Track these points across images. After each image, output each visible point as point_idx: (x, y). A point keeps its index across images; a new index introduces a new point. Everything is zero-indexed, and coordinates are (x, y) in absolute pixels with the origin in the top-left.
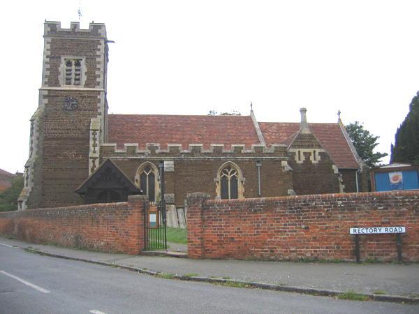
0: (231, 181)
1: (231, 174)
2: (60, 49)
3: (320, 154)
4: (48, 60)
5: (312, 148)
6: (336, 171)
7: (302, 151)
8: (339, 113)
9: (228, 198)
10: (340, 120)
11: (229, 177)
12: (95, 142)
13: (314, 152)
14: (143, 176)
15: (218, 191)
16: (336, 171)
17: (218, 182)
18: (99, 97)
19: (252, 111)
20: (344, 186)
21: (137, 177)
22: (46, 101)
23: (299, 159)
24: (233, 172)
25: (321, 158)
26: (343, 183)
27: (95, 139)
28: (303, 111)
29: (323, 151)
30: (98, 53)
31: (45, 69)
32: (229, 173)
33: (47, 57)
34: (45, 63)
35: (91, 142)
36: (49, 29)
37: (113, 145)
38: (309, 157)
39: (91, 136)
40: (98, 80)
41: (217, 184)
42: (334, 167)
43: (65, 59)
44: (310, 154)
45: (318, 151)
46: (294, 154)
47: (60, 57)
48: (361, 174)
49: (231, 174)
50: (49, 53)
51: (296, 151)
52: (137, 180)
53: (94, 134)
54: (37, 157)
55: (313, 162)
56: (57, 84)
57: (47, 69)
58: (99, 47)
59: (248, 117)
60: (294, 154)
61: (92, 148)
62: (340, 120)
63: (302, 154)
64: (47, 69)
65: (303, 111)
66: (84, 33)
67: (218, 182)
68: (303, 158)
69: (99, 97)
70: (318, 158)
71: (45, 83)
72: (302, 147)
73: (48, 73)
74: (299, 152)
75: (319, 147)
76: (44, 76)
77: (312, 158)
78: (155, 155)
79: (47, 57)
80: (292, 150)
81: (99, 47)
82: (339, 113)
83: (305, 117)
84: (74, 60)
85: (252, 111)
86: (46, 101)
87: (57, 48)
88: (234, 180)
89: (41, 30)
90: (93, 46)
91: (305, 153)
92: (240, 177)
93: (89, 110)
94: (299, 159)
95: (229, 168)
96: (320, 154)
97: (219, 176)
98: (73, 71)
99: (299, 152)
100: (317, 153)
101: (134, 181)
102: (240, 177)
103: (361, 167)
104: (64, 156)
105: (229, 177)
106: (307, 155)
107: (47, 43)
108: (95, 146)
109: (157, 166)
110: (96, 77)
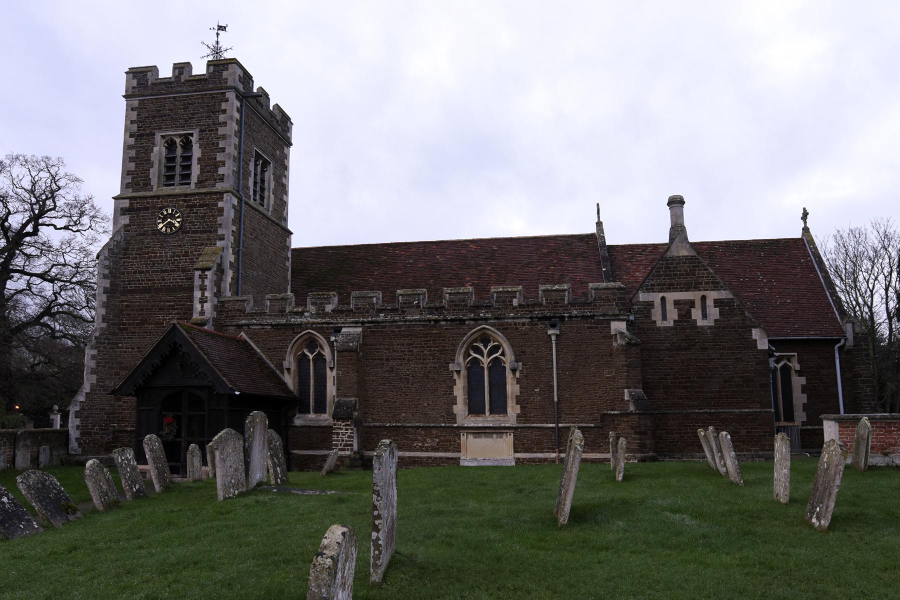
0: (490, 369)
1: (489, 355)
2: (154, 117)
3: (718, 303)
4: (132, 141)
5: (697, 288)
6: (763, 344)
7: (672, 296)
8: (805, 215)
9: (839, 413)
10: (806, 230)
11: (485, 361)
12: (203, 294)
13: (704, 298)
14: (302, 361)
15: (459, 390)
16: (763, 344)
17: (458, 372)
18: (220, 204)
19: (599, 224)
20: (802, 380)
21: (290, 361)
22: (125, 220)
23: (664, 318)
24: (495, 349)
25: (721, 313)
26: (800, 373)
27: (203, 288)
28: (676, 203)
29: (724, 294)
30: (222, 118)
31: (127, 159)
32: (485, 352)
33: (131, 136)
34: (127, 147)
35: (197, 294)
36: (135, 83)
37: (794, 354)
38: (689, 313)
39: (197, 282)
40: (221, 171)
41: (455, 376)
42: (756, 334)
43: (163, 137)
44: (692, 304)
45: (712, 295)
46: (651, 304)
47: (154, 134)
48: (849, 352)
49: (489, 355)
50: (135, 127)
51: (656, 297)
52: (289, 370)
53: (203, 278)
54: (104, 325)
55: (700, 323)
56: (147, 185)
57: (131, 159)
58: (224, 106)
59: (591, 236)
60: (651, 304)
61: (198, 306)
62: (806, 230)
63: (670, 306)
64: (131, 159)
65: (676, 203)
66: (200, 80)
67: (458, 372)
68: (673, 314)
69: (220, 204)
70: (714, 313)
71: (125, 186)
72: (671, 288)
73: (132, 166)
74: (663, 299)
75: (716, 287)
76: (126, 173)
77: (696, 314)
78: (326, 315)
79: (131, 136)
80: (643, 297)
81: (224, 106)
82: (805, 215)
83: (681, 215)
84: (180, 135)
85: (599, 224)
86: (125, 220)
87: (148, 117)
88: (497, 365)
89: (120, 85)
90: (214, 105)
91: (677, 303)
92: (509, 359)
93: (202, 232)
94: (664, 318)
95: (486, 342)
96: (718, 303)
97: (460, 359)
98: (179, 160)
99: (663, 299)
100: (710, 303)
101: (283, 373)
102: (509, 359)
103: (850, 335)
104: (156, 324)
105: (485, 361)
106: (685, 307)
107: (130, 109)
108: (203, 301)
109: (328, 339)
110: (217, 165)
